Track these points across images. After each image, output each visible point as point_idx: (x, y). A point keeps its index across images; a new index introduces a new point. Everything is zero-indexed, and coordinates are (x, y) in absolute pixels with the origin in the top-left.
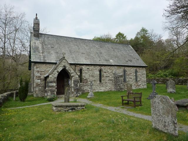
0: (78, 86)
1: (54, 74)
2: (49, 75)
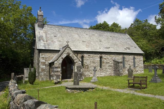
0: (81, 71)
1: (59, 61)
2: (54, 62)
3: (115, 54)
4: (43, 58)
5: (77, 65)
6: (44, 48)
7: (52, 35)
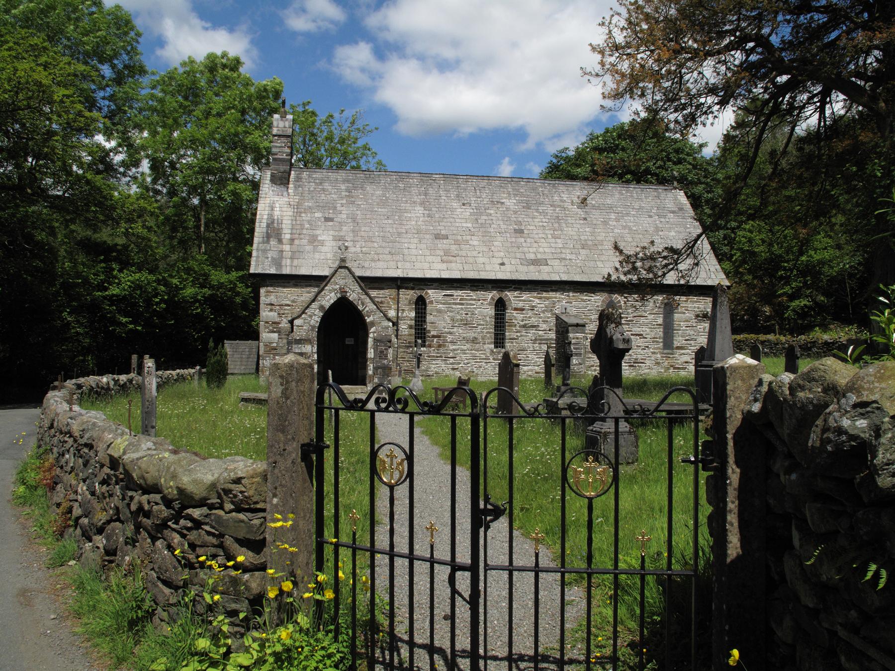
1: (311, 316)
3: (568, 291)
4: (269, 307)
5: (374, 332)
6: (273, 271)
7: (317, 215)
